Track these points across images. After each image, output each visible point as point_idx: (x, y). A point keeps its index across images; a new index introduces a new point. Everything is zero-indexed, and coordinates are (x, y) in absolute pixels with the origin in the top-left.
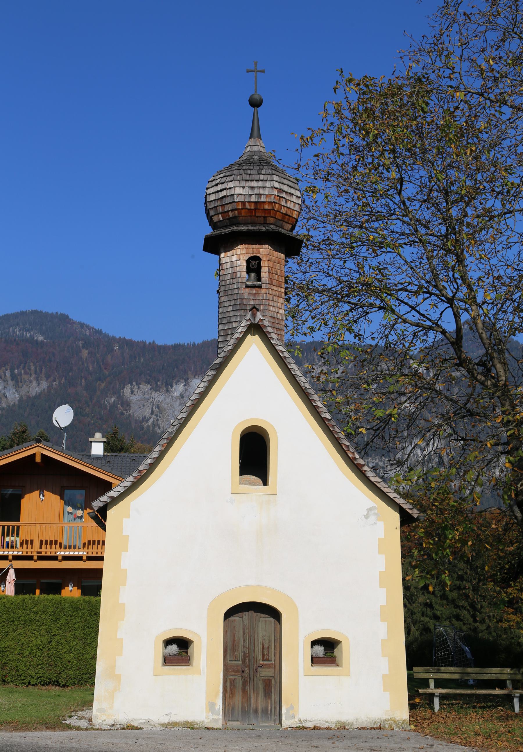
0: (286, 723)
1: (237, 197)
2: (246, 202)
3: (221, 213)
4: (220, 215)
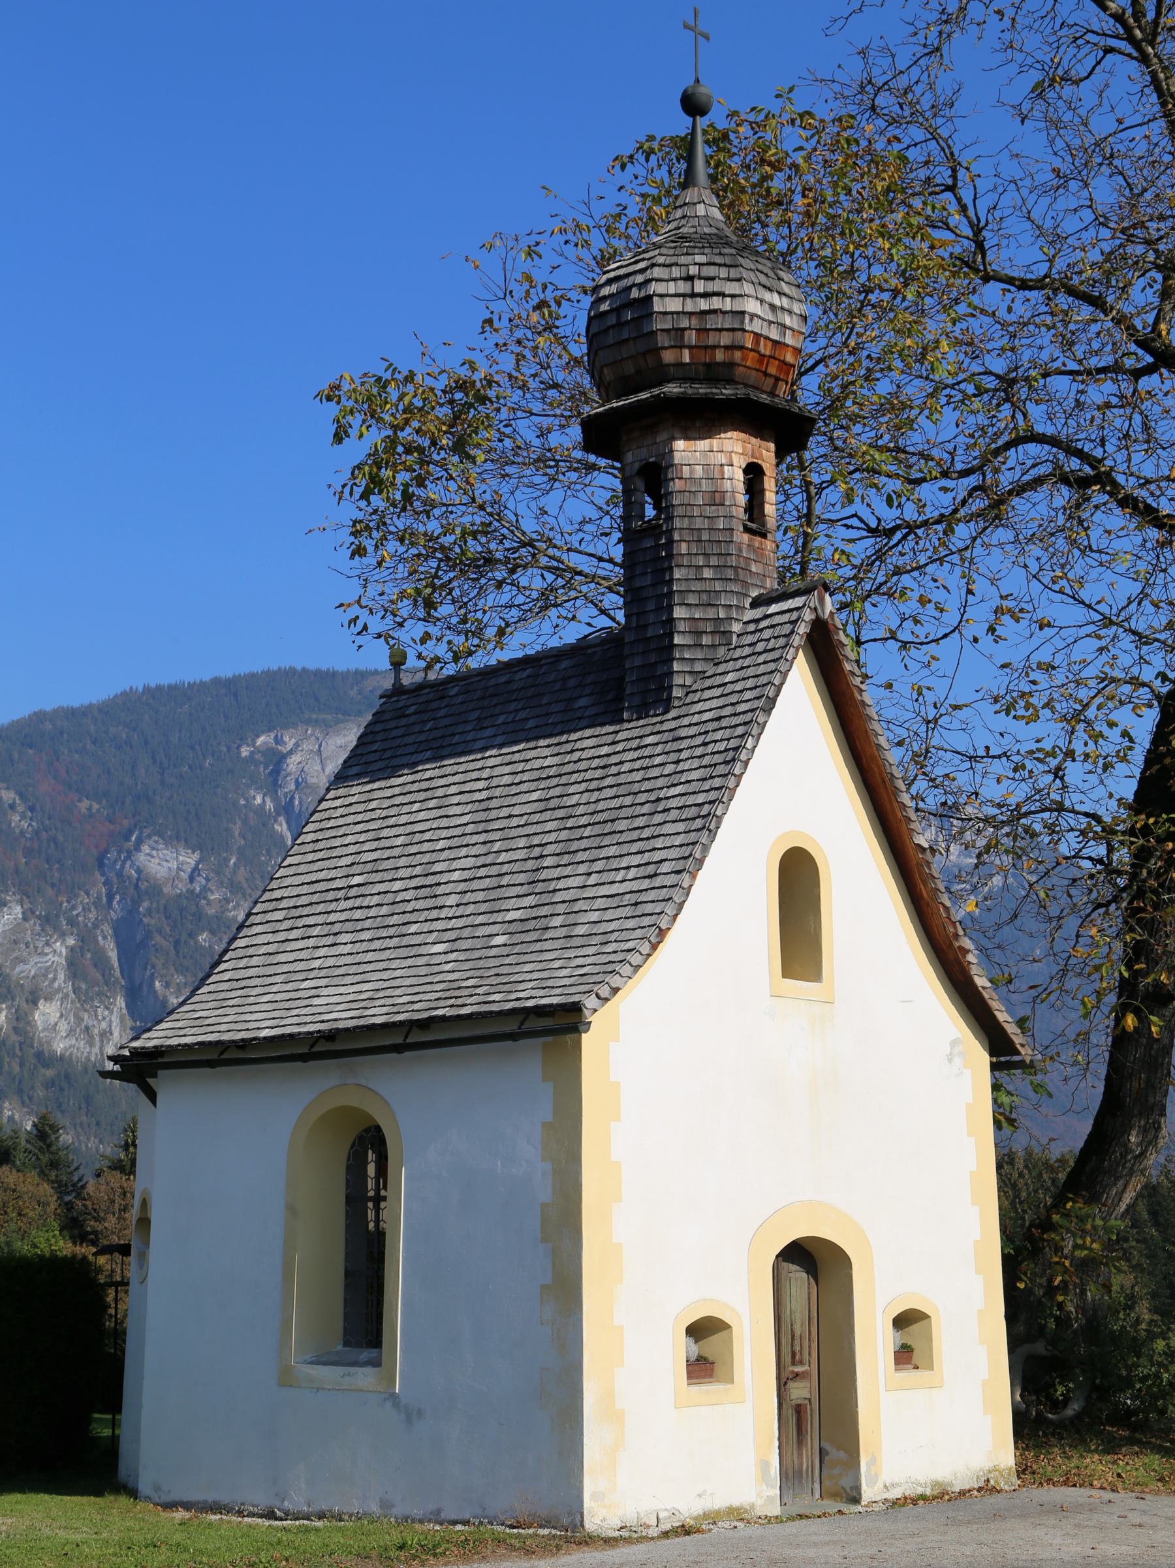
0: (870, 1492)
1: (751, 320)
2: (761, 335)
3: (690, 347)
4: (686, 352)
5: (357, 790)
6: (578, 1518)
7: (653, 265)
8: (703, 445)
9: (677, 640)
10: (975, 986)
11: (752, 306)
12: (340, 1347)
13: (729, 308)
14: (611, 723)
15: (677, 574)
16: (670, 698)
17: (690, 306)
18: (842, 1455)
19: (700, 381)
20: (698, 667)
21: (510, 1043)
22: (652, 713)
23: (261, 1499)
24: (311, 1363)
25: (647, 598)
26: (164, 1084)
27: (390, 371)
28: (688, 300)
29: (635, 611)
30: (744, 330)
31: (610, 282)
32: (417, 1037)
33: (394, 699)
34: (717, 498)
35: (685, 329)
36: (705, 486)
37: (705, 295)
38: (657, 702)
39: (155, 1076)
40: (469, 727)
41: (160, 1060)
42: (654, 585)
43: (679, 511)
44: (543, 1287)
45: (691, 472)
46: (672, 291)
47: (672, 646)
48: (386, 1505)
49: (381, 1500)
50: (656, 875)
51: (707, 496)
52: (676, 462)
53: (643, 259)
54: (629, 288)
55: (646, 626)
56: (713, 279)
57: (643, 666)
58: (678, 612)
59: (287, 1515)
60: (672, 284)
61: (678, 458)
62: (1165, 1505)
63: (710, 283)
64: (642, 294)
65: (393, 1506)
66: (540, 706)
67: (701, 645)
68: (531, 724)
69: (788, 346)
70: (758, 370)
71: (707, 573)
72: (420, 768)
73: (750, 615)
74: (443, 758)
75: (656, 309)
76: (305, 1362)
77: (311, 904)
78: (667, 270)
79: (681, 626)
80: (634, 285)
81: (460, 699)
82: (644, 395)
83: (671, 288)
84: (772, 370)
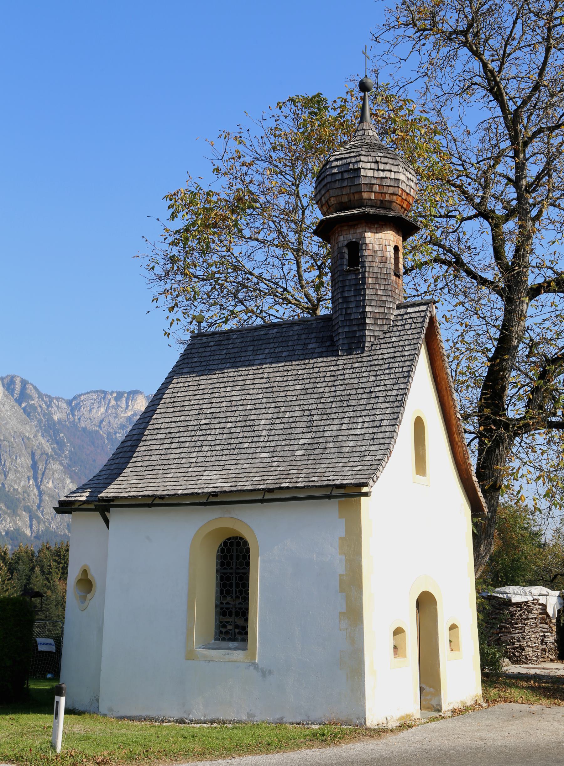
0: (446, 707)
3: (375, 192)
4: (373, 194)
5: (191, 380)
6: (363, 721)
7: (360, 155)
8: (378, 235)
9: (367, 321)
10: (473, 481)
11: (402, 177)
12: (213, 641)
13: (393, 177)
14: (332, 356)
15: (367, 292)
16: (364, 347)
17: (377, 174)
18: (432, 689)
19: (379, 208)
20: (376, 334)
21: (327, 500)
22: (354, 353)
23: (177, 715)
24: (203, 648)
25: (351, 301)
26: (114, 515)
27: (198, 189)
28: (376, 172)
29: (345, 306)
30: (399, 187)
31: (337, 160)
32: (268, 496)
33: (199, 338)
34: (384, 260)
35: (374, 184)
36: (379, 254)
37: (383, 170)
38: (357, 348)
39: (108, 511)
40: (248, 354)
41: (112, 503)
42: (355, 296)
43: (368, 264)
44: (341, 613)
45: (373, 247)
46: (369, 167)
47: (365, 323)
48: (250, 715)
49: (248, 714)
50: (380, 426)
51: (380, 258)
52: (367, 242)
53: (354, 152)
54: (349, 164)
55: (350, 314)
56: (386, 164)
57: (349, 332)
58: (368, 309)
59: (192, 722)
60: (369, 164)
61: (367, 241)
62: (560, 709)
63: (385, 165)
64: (355, 167)
65: (255, 716)
66: (288, 346)
67: (377, 324)
68: (285, 354)
69: (411, 195)
70: (400, 205)
71: (380, 292)
72: (226, 371)
73: (397, 312)
74: (238, 367)
75: (362, 174)
76: (200, 648)
77: (179, 432)
78: (366, 158)
79: (369, 315)
80: (351, 163)
81: (239, 340)
82: (355, 211)
83: (369, 166)
84: (405, 206)
